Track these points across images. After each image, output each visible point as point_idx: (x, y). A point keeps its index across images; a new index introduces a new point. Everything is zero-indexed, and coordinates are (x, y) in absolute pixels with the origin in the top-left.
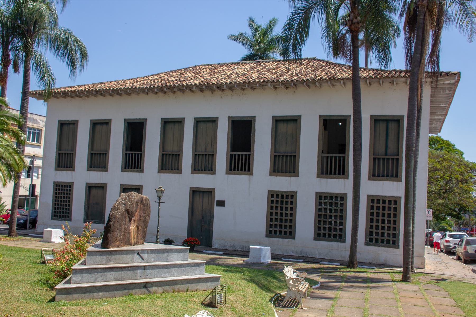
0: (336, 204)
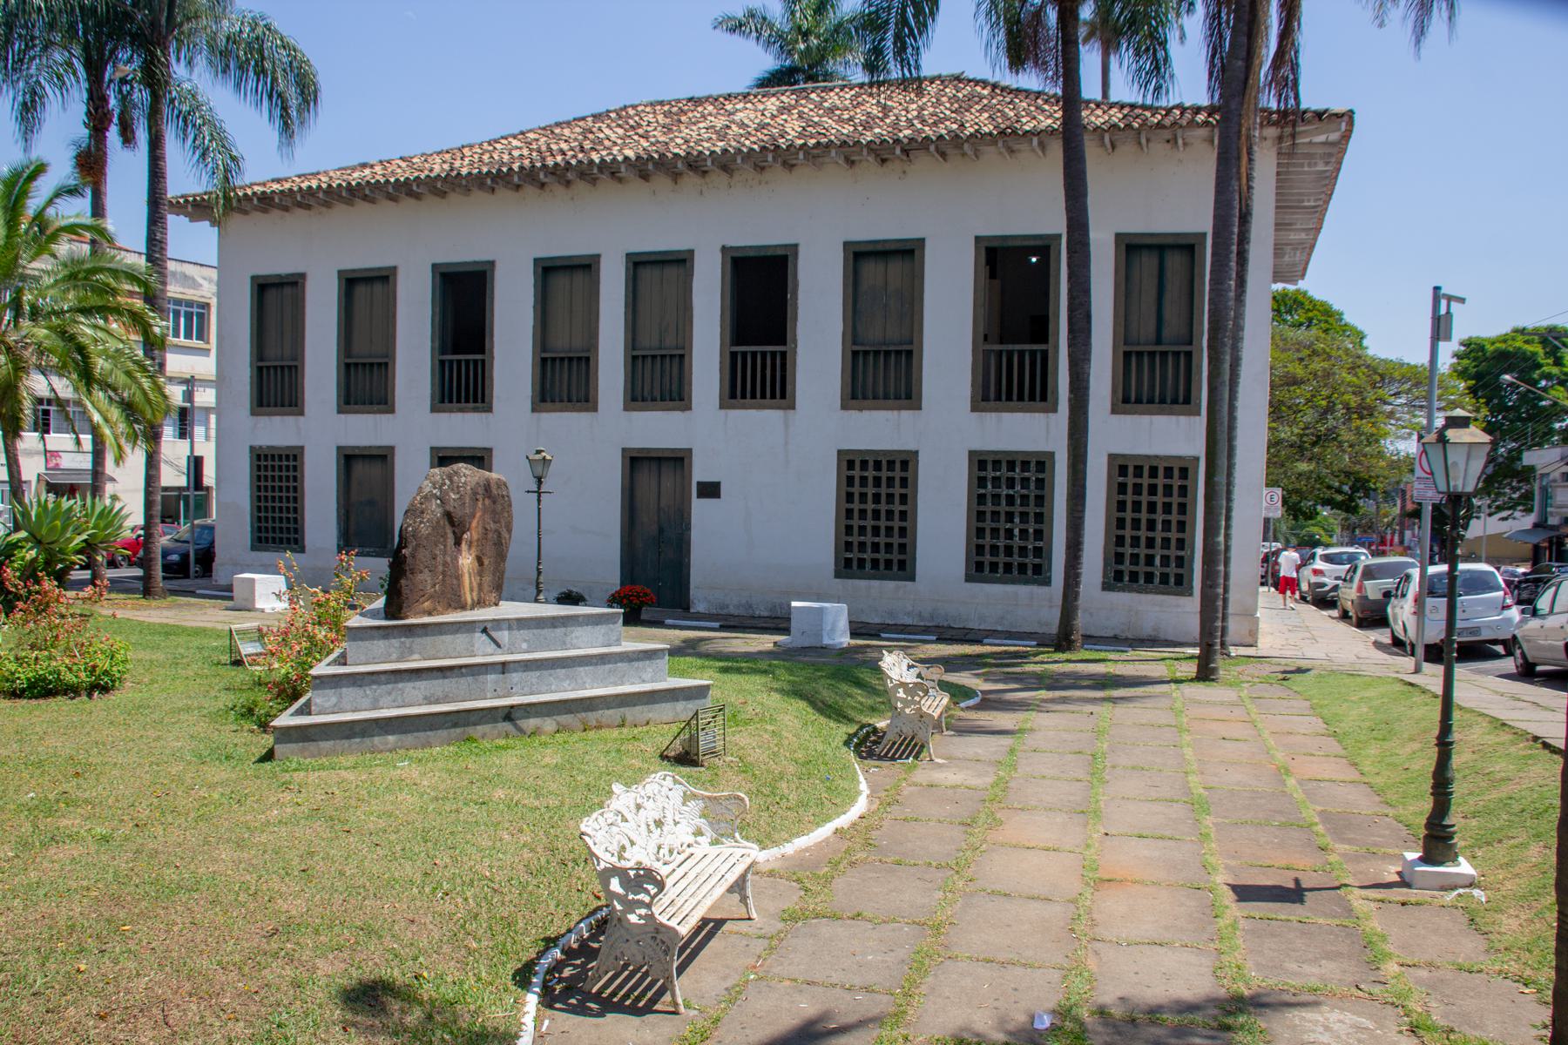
0: (1025, 481)
